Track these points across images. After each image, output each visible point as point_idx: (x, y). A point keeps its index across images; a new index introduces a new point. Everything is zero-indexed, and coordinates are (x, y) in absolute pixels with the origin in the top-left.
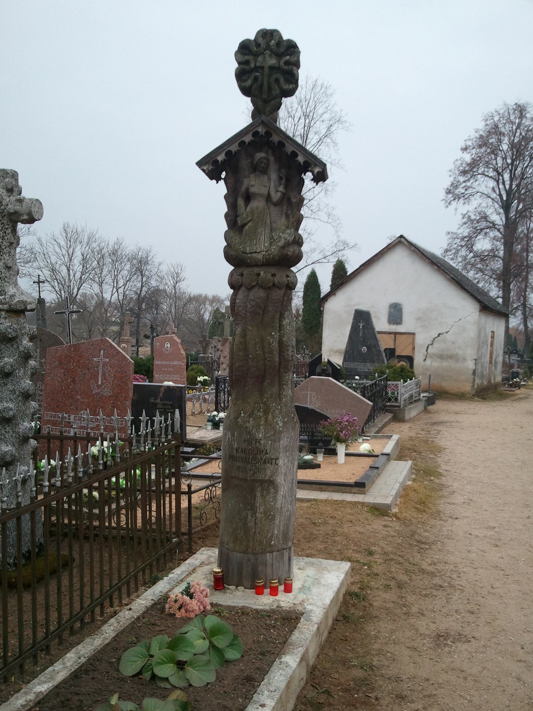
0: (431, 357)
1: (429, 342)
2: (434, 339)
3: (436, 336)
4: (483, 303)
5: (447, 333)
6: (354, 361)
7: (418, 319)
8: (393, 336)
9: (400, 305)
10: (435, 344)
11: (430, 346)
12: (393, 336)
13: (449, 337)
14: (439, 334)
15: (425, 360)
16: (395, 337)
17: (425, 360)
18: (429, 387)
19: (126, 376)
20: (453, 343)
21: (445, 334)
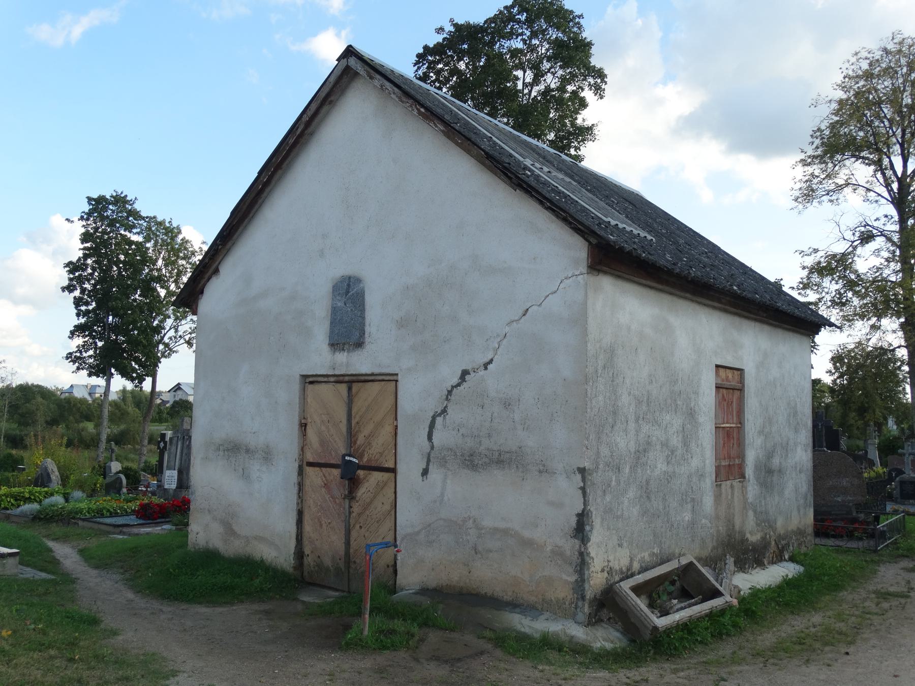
0: (443, 462)
1: (433, 405)
2: (450, 392)
3: (455, 380)
4: (594, 233)
5: (486, 366)
6: (741, 467)
7: (402, 324)
8: (343, 388)
9: (359, 280)
10: (455, 415)
11: (439, 420)
12: (343, 388)
13: (493, 382)
14: (465, 373)
15: (425, 472)
16: (350, 389)
17: (425, 472)
18: (299, 554)
19: (676, 649)
20: (507, 404)
21: (482, 372)
